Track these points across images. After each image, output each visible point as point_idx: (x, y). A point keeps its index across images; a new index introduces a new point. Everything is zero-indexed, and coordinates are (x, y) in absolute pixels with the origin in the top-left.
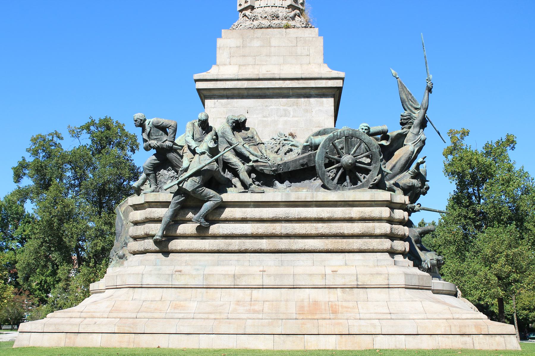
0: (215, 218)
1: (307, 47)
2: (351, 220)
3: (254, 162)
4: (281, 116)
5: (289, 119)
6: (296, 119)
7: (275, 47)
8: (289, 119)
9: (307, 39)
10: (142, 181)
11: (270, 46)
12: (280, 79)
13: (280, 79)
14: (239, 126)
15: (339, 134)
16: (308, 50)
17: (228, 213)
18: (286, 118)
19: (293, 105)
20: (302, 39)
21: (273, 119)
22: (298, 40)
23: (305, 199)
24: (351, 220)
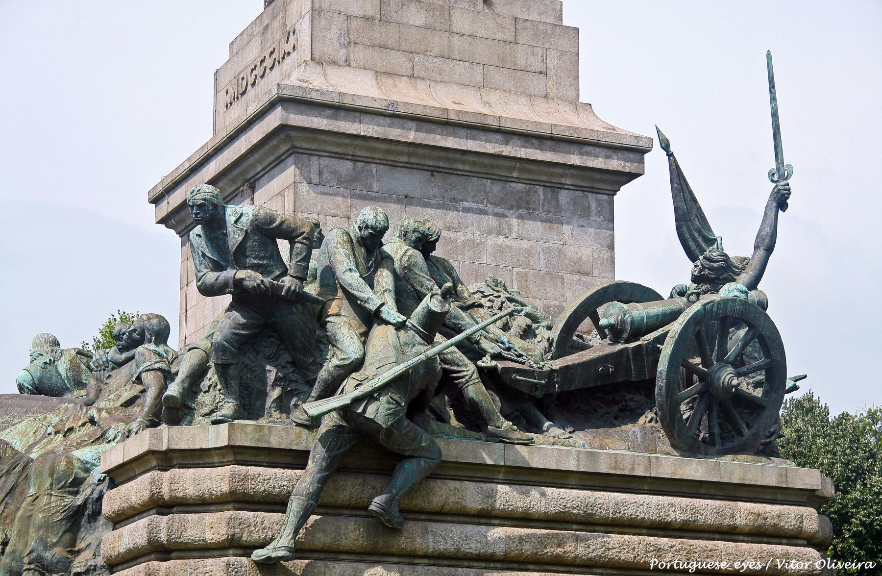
0: (419, 502)
1: (539, 51)
2: (730, 533)
3: (495, 357)
4: (489, 233)
5: (508, 242)
6: (525, 244)
7: (462, 35)
8: (508, 242)
9: (541, 27)
10: (553, 509)
11: (451, 32)
12: (218, 150)
13: (218, 150)
14: (425, 244)
15: (715, 309)
16: (545, 60)
17: (446, 492)
18: (500, 240)
19: (519, 207)
20: (527, 24)
21: (470, 236)
22: (519, 27)
23: (633, 469)
24: (730, 533)
